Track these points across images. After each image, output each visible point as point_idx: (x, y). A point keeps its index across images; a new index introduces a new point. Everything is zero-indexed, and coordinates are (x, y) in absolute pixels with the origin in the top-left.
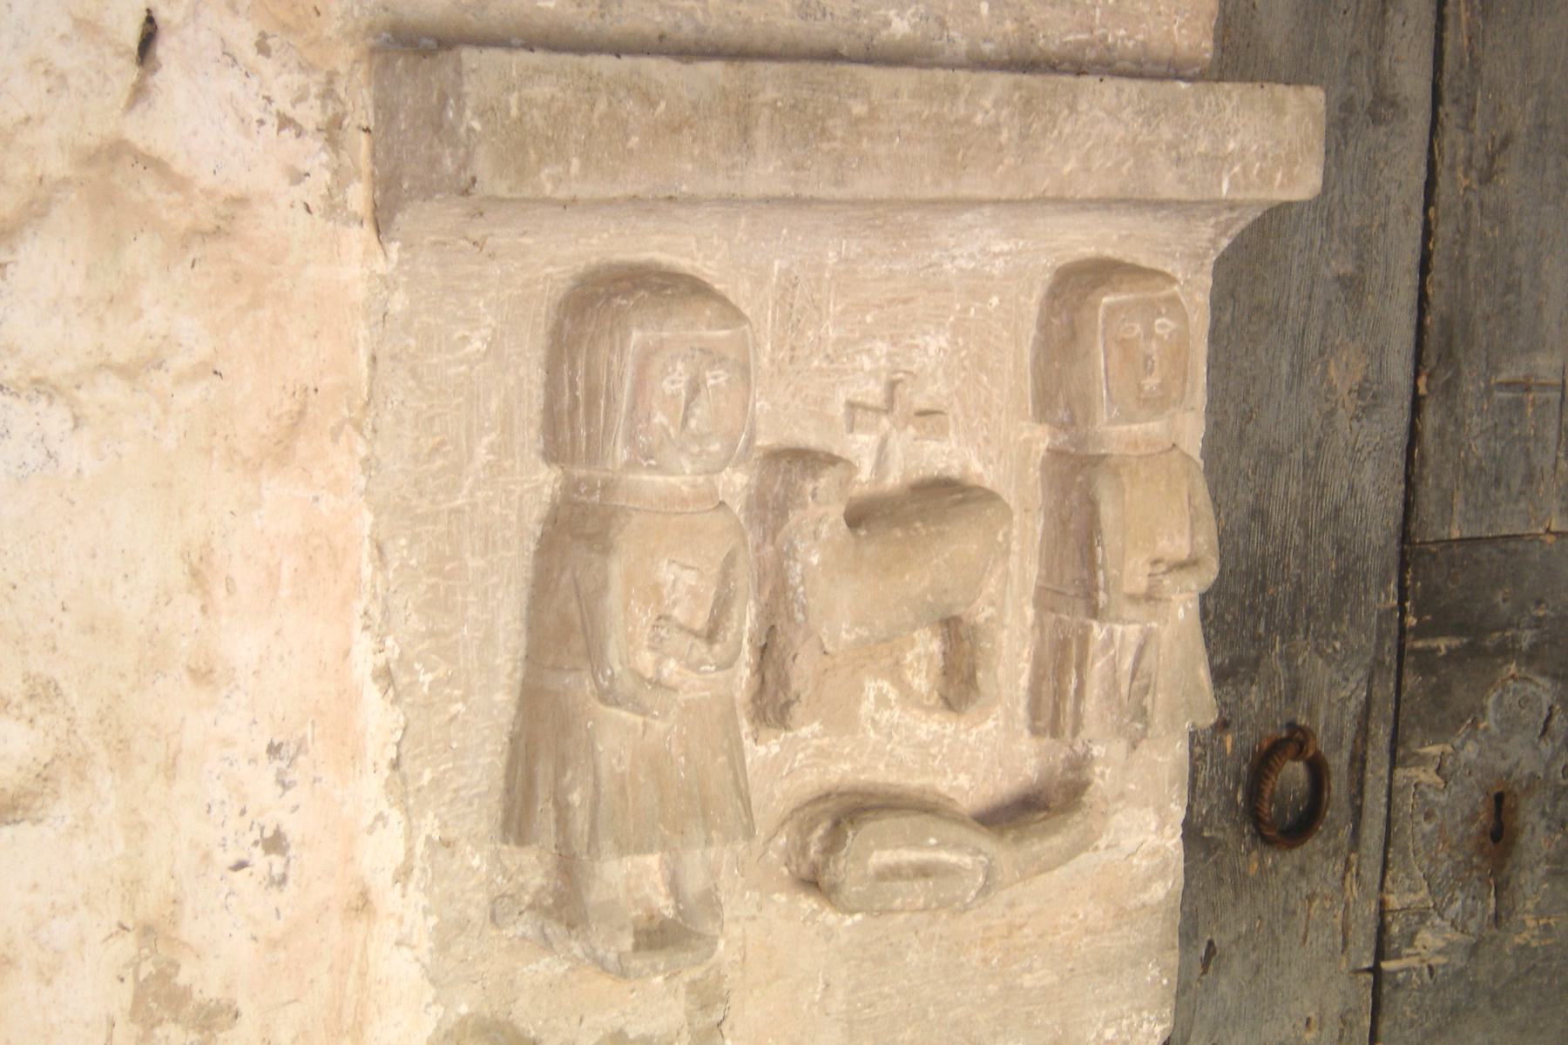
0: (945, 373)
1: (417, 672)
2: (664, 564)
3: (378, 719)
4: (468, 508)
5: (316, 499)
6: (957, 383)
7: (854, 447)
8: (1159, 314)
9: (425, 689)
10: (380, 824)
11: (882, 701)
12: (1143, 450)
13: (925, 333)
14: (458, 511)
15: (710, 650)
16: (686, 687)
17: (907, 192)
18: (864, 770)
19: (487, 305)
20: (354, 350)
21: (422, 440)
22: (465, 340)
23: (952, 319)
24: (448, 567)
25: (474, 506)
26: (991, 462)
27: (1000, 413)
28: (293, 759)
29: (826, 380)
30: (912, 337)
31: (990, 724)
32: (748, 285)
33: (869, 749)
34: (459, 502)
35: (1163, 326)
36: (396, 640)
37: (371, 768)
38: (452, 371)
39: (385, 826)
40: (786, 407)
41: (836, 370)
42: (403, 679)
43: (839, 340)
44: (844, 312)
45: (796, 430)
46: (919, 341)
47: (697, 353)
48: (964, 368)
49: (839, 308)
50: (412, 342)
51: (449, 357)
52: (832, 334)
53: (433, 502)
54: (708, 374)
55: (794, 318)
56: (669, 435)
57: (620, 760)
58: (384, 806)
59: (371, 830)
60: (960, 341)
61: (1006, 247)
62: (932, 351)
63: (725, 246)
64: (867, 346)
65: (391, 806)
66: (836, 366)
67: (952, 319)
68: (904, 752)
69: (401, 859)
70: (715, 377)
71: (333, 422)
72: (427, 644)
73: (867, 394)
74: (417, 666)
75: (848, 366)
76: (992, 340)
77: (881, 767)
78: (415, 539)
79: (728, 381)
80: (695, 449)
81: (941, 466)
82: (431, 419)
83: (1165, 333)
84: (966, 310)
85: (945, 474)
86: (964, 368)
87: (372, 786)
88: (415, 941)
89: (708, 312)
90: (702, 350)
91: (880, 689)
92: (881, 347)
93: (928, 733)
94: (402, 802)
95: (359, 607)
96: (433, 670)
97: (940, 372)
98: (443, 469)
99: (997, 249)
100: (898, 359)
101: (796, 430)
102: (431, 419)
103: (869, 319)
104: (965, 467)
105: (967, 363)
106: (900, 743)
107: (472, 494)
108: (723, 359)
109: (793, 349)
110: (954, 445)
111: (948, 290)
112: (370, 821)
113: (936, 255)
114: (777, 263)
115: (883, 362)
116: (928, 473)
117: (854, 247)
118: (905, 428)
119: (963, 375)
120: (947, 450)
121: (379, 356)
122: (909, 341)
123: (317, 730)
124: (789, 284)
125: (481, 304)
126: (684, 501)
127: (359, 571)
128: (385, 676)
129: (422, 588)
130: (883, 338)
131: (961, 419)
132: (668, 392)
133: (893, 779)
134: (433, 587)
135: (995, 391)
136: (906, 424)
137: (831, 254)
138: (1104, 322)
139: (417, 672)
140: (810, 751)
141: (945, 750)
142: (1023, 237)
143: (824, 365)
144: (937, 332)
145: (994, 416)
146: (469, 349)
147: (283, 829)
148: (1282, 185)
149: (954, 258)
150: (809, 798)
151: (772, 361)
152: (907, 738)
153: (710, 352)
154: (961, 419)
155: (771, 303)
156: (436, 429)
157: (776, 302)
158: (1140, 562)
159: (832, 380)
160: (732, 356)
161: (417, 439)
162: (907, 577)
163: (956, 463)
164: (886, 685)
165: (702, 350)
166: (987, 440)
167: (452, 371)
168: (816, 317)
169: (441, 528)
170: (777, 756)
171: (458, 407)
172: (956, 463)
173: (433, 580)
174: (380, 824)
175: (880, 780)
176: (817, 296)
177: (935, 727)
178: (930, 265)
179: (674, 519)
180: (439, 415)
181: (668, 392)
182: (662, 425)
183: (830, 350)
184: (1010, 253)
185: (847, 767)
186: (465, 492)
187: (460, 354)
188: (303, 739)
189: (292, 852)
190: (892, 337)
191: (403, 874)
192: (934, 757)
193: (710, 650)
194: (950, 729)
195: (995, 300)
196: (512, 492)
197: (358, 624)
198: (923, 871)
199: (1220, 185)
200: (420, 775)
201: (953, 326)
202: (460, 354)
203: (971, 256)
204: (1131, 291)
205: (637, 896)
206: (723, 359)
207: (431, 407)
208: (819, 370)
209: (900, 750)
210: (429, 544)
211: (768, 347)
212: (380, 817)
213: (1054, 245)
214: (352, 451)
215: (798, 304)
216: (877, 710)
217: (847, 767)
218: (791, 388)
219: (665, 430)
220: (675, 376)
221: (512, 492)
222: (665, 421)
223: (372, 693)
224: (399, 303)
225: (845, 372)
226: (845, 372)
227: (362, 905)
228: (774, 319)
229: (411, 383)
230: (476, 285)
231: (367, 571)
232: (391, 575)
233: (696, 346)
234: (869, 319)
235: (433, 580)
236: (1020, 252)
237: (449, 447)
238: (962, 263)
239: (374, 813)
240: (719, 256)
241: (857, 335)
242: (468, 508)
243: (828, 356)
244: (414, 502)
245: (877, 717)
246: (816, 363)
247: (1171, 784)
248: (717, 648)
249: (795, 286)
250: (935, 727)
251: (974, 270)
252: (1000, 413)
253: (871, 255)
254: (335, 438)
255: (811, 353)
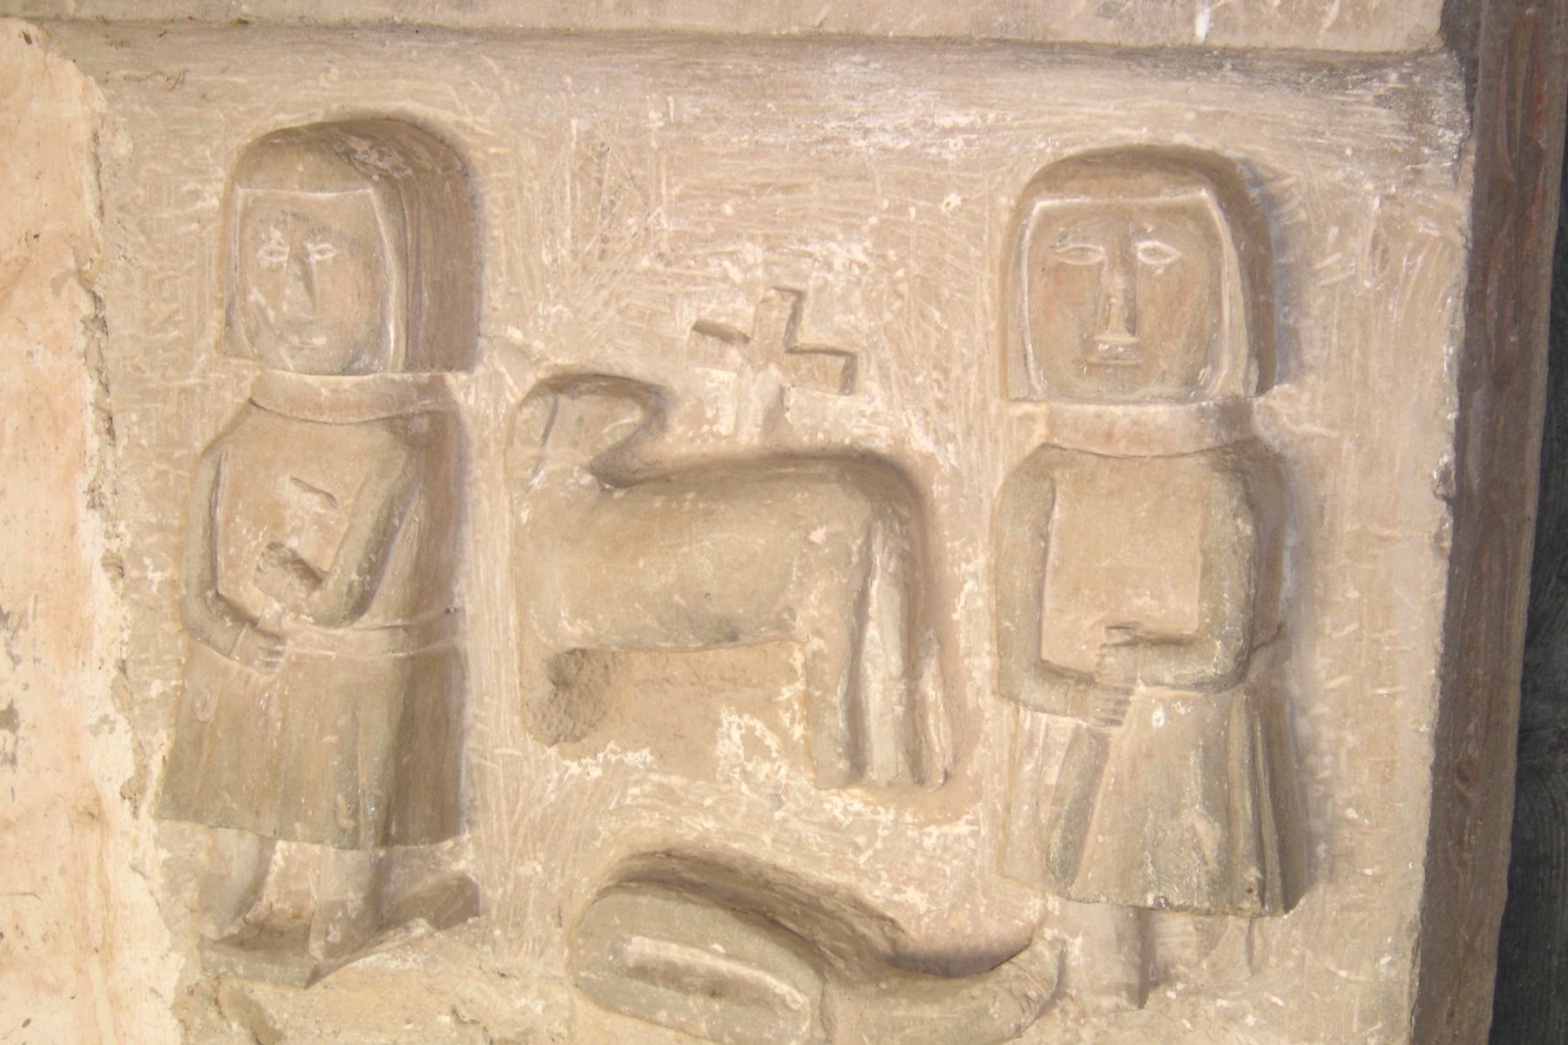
0: (866, 300)
1: (146, 568)
2: (285, 480)
3: (106, 607)
4: (199, 390)
5: (30, 354)
6: (887, 316)
7: (709, 385)
8: (1142, 233)
9: (154, 589)
10: (106, 728)
11: (754, 745)
12: (1121, 448)
13: (825, 237)
14: (186, 391)
15: (309, 595)
16: (300, 638)
17: (577, 19)
18: (738, 836)
19: (215, 155)
20: (79, 196)
21: (153, 305)
22: (196, 195)
23: (873, 220)
24: (177, 454)
25: (206, 387)
26: (951, 437)
27: (966, 368)
28: (15, 631)
29: (660, 288)
30: (803, 241)
31: (962, 828)
32: (533, 151)
33: (743, 809)
34: (192, 381)
35: (1153, 252)
36: (127, 526)
37: (96, 664)
38: (183, 229)
39: (112, 730)
40: (594, 319)
41: (679, 277)
42: (133, 573)
43: (679, 235)
44: (682, 198)
45: (609, 350)
46: (815, 248)
47: (289, 219)
48: (901, 296)
49: (677, 190)
50: (140, 191)
51: (178, 212)
52: (668, 226)
53: (163, 376)
54: (309, 246)
55: (605, 199)
56: (266, 318)
57: (205, 705)
58: (109, 709)
59: (95, 731)
60: (891, 253)
61: (963, 121)
62: (837, 265)
63: (496, 98)
64: (730, 248)
65: (118, 711)
66: (675, 269)
67: (873, 220)
68: (811, 835)
69: (130, 772)
70: (320, 252)
71: (55, 272)
72: (154, 539)
73: (735, 314)
74: (147, 561)
75: (698, 273)
76: (948, 257)
77: (767, 838)
78: (145, 416)
79: (335, 259)
80: (296, 340)
81: (858, 432)
82: (161, 282)
83: (1159, 265)
84: (901, 209)
85: (865, 445)
86: (901, 296)
87: (96, 682)
88: (148, 869)
89: (300, 168)
90: (294, 215)
91: (751, 729)
92: (753, 253)
93: (845, 811)
94: (126, 708)
95: (84, 481)
96: (163, 569)
97: (857, 298)
98: (178, 340)
99: (947, 122)
100: (777, 270)
101: (609, 350)
102: (161, 282)
103: (728, 209)
104: (901, 441)
105: (903, 288)
106: (796, 814)
107: (204, 374)
108: (324, 230)
109: (605, 240)
110: (880, 404)
111: (862, 176)
112: (94, 721)
113: (832, 125)
114: (574, 122)
115: (760, 272)
116: (836, 439)
117: (689, 108)
118: (766, 365)
119: (898, 304)
120: (869, 410)
121: (107, 205)
122: (796, 246)
123: (40, 607)
124: (594, 154)
125: (208, 153)
126: (319, 407)
127: (83, 442)
128: (116, 566)
129: (151, 473)
130: (752, 238)
131: (894, 368)
132: (265, 264)
133: (786, 861)
134: (162, 474)
135: (958, 334)
136: (768, 360)
137: (653, 115)
138: (1033, 238)
139: (146, 568)
140: (648, 788)
141: (879, 845)
142: (991, 107)
143: (660, 267)
144: (849, 239)
145: (956, 371)
146: (199, 205)
147: (16, 706)
148: (1338, 25)
149: (867, 132)
150: (644, 850)
151: (574, 254)
152: (808, 811)
153: (305, 219)
154: (894, 368)
155: (568, 177)
156: (165, 294)
157: (574, 175)
158: (1086, 623)
159: (670, 289)
160: (336, 225)
161: (148, 303)
162: (641, 564)
163: (883, 430)
164: (759, 727)
165: (294, 215)
166: (941, 406)
167: (183, 229)
168: (639, 201)
169: (171, 408)
170: (597, 782)
171: (189, 272)
172: (883, 430)
173: (164, 467)
174: (106, 728)
175: (764, 858)
176: (638, 172)
177: (857, 806)
178: (826, 140)
179: (296, 427)
180: (169, 278)
181: (265, 264)
182: (258, 304)
183: (664, 247)
184: (971, 129)
185: (710, 824)
186: (196, 370)
187: (189, 210)
188: (24, 614)
189: (21, 732)
190: (767, 237)
191: (132, 793)
192: (858, 849)
193: (309, 595)
194: (886, 816)
195: (954, 199)
196: (245, 377)
197: (82, 501)
198: (717, 988)
199: (1191, 20)
200: (147, 684)
201: (876, 231)
202: (189, 210)
203: (901, 131)
204: (1085, 191)
205: (294, 887)
206: (324, 230)
207: (161, 268)
208: (650, 274)
209: (794, 824)
210: (158, 426)
211: (568, 234)
212: (105, 719)
213: (1057, 120)
214: (74, 307)
215: (609, 180)
216: (749, 759)
217: (710, 824)
218: (604, 294)
219: (262, 311)
220: (273, 245)
221: (245, 377)
222: (262, 301)
223: (101, 580)
224: (122, 146)
225: (693, 280)
226: (693, 280)
227: (94, 816)
228: (574, 199)
229: (142, 239)
230: (199, 131)
231: (93, 444)
232: (120, 452)
233: (289, 208)
234: (728, 209)
235: (164, 467)
236: (990, 130)
237: (180, 317)
238: (886, 140)
239: (99, 714)
240: (491, 109)
241: (711, 229)
242: (199, 390)
243: (661, 255)
244: (148, 375)
245: (750, 767)
246: (645, 263)
247: (1368, 1019)
248: (317, 595)
249: (601, 155)
250: (857, 806)
251: (907, 150)
252: (966, 368)
253: (719, 120)
254: (57, 291)
255: (635, 248)
